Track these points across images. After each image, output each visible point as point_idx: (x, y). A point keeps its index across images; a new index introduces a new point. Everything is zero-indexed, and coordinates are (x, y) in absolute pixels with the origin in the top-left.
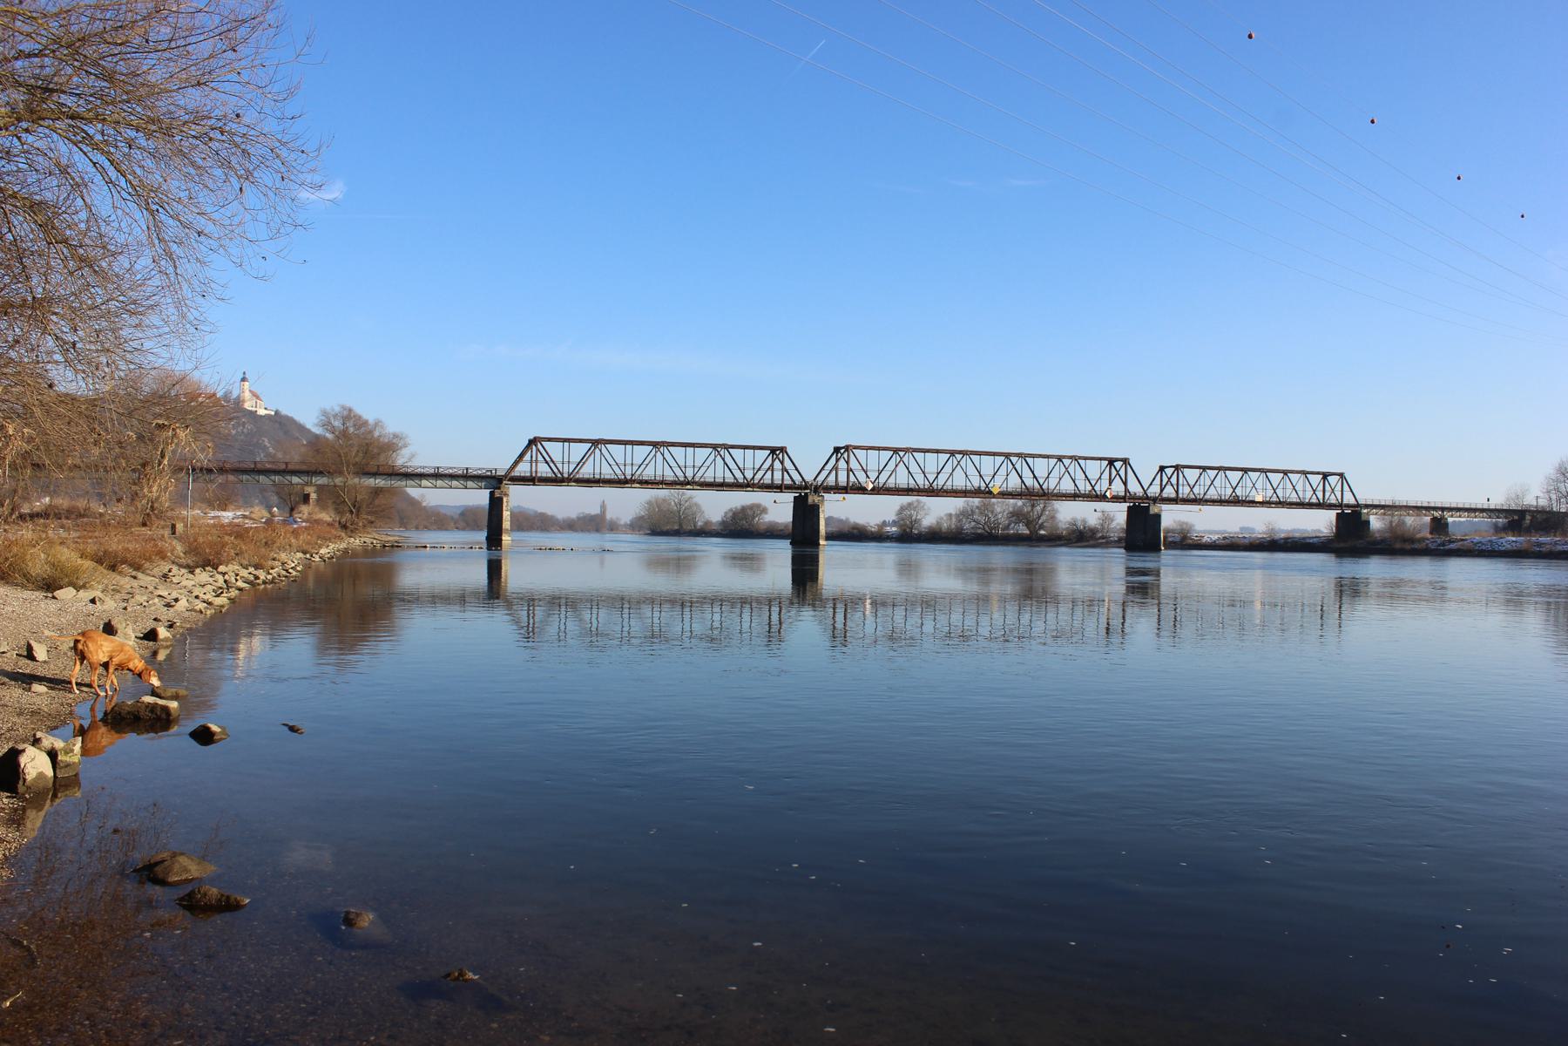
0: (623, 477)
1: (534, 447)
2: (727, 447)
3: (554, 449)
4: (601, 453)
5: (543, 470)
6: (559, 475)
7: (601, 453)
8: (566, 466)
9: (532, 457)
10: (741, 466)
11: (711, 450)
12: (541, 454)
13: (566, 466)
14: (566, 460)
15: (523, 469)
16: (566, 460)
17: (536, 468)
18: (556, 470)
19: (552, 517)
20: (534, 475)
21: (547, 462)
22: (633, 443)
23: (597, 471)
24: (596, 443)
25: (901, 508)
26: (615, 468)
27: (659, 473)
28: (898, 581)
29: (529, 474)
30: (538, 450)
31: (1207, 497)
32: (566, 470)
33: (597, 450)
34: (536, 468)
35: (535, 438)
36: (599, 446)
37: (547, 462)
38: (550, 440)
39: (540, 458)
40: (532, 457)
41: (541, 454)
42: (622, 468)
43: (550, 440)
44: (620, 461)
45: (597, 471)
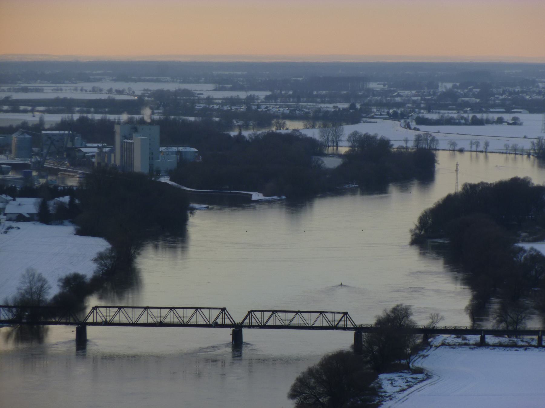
0: (260, 324)
1: (250, 314)
2: (200, 308)
3: (258, 315)
4: (299, 316)
5: (254, 323)
6: (355, 326)
7: (299, 316)
8: (185, 319)
9: (222, 316)
10: (123, 314)
11: (169, 309)
12: (324, 318)
13: (185, 319)
14: (185, 316)
15: (247, 322)
16: (185, 316)
17: (345, 323)
18: (330, 323)
19: (89, 325)
20: (346, 326)
21: (255, 320)
22: (264, 311)
23: (198, 321)
24: (274, 312)
25: (526, 349)
26: (154, 318)
27: (121, 320)
28: (209, 363)
29: (344, 326)
30: (252, 315)
31: (339, 326)
32: (185, 321)
33: (197, 311)
34: (345, 323)
35: (96, 306)
36: (147, 309)
37: (255, 320)
38: (257, 311)
39: (348, 320)
40: (222, 316)
41: (324, 318)
42: (131, 318)
43: (257, 311)
44: (105, 314)
45: (198, 321)
